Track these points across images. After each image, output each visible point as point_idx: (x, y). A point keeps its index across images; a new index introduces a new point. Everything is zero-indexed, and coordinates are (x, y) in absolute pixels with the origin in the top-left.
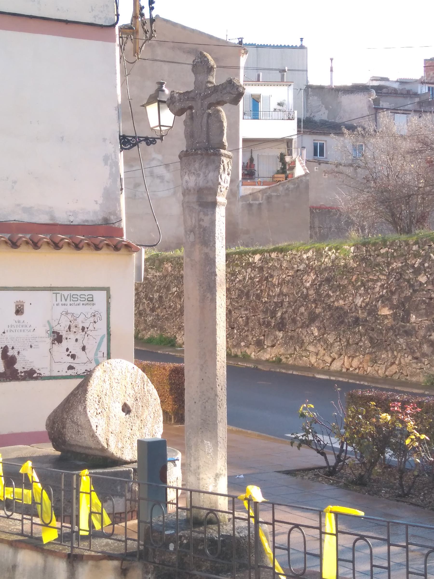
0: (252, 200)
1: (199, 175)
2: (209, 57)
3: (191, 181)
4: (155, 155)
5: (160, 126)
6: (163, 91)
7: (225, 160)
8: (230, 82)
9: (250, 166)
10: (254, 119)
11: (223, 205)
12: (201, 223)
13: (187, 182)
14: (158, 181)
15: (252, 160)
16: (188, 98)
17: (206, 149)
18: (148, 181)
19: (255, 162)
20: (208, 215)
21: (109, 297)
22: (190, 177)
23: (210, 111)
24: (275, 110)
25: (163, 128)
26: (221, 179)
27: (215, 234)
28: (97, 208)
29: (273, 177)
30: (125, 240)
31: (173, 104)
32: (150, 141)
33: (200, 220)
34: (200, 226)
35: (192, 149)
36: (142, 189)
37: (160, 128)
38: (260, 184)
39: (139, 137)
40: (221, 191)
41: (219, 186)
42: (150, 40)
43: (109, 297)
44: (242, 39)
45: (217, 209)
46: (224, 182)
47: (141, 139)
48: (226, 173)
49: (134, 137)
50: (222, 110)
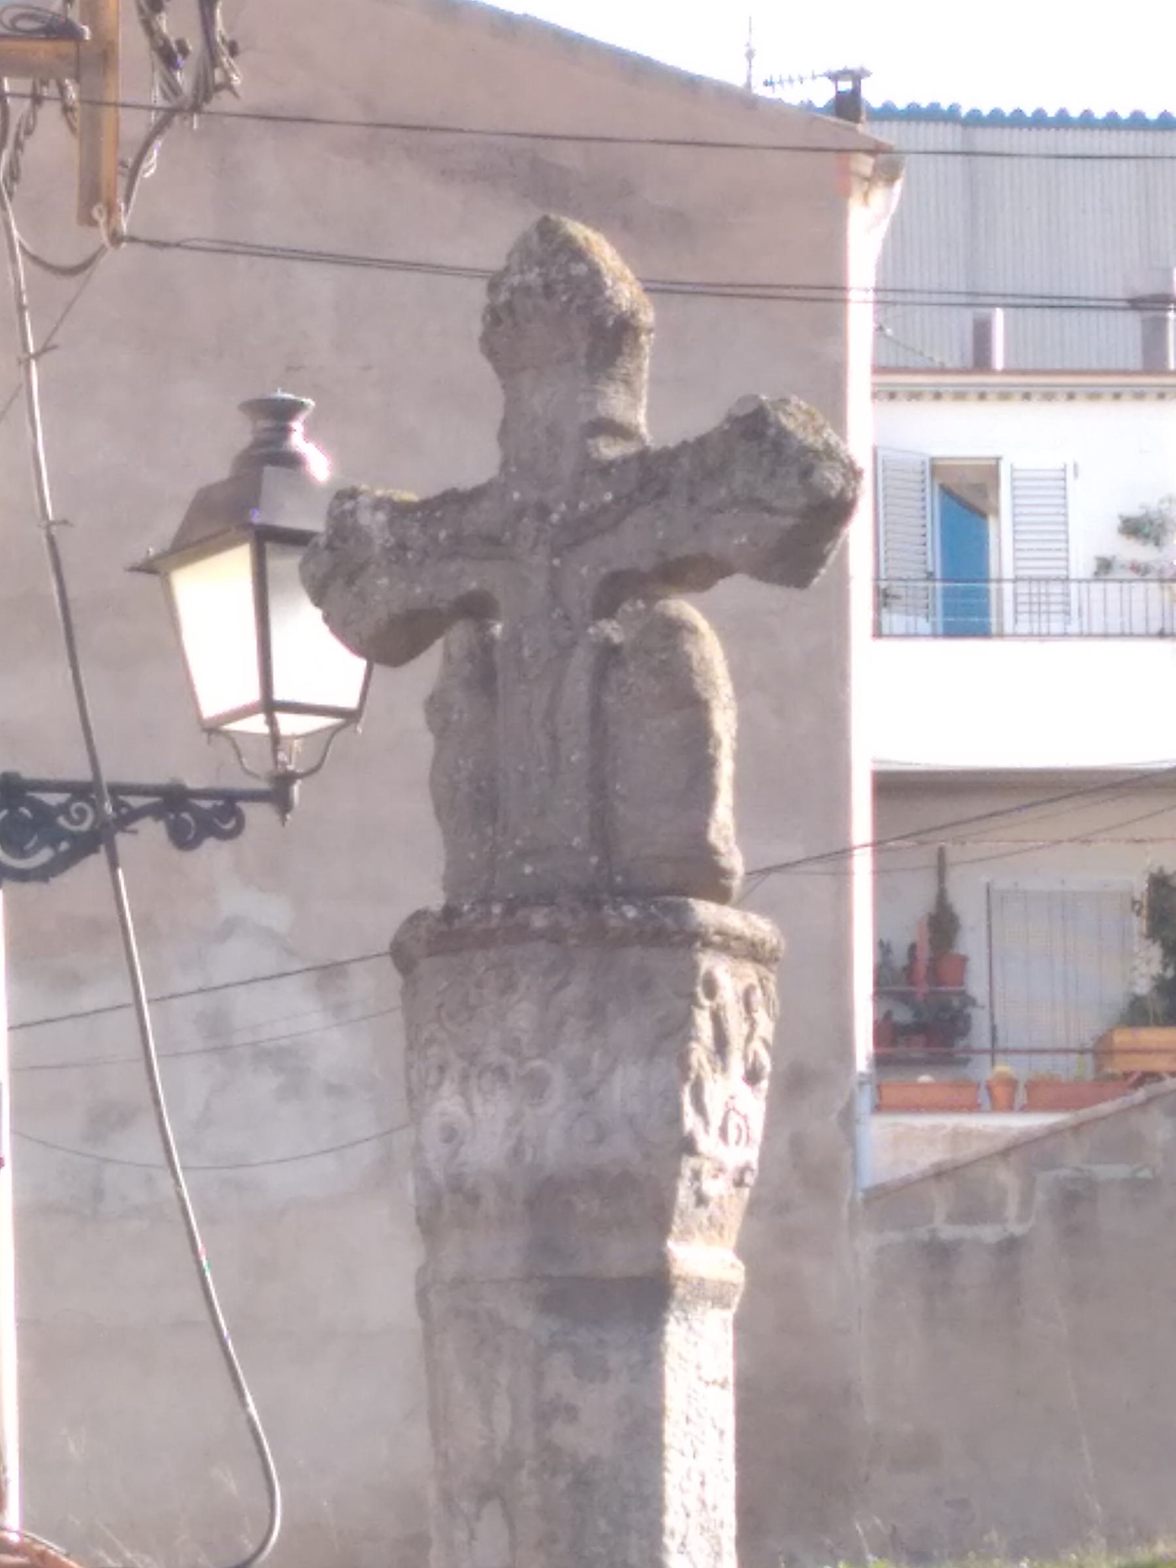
0: (952, 1219)
1: (537, 1086)
2: (606, 254)
3: (484, 1126)
4: (236, 900)
5: (269, 706)
6: (293, 461)
7: (729, 977)
8: (754, 428)
9: (935, 973)
10: (952, 632)
11: (720, 1301)
12: (564, 1434)
13: (450, 1135)
14: (266, 1083)
15: (943, 924)
16: (457, 539)
17: (592, 897)
18: (184, 1086)
19: (971, 943)
20: (605, 1373)
22: (477, 1100)
23: (613, 630)
24: (1105, 567)
25: (289, 724)
26: (700, 1108)
27: (660, 1510)
29: (1102, 1050)
30: (14, 1538)
31: (350, 580)
32: (196, 816)
33: (550, 1412)
34: (551, 1457)
35: (485, 900)
36: (138, 1144)
37: (272, 722)
38: (1004, 1097)
39: (117, 790)
40: (701, 1200)
41: (688, 1164)
42: (196, 108)
44: (857, 77)
45: (675, 1332)
46: (723, 1132)
47: (136, 802)
48: (737, 1066)
49: (81, 791)
50: (703, 625)
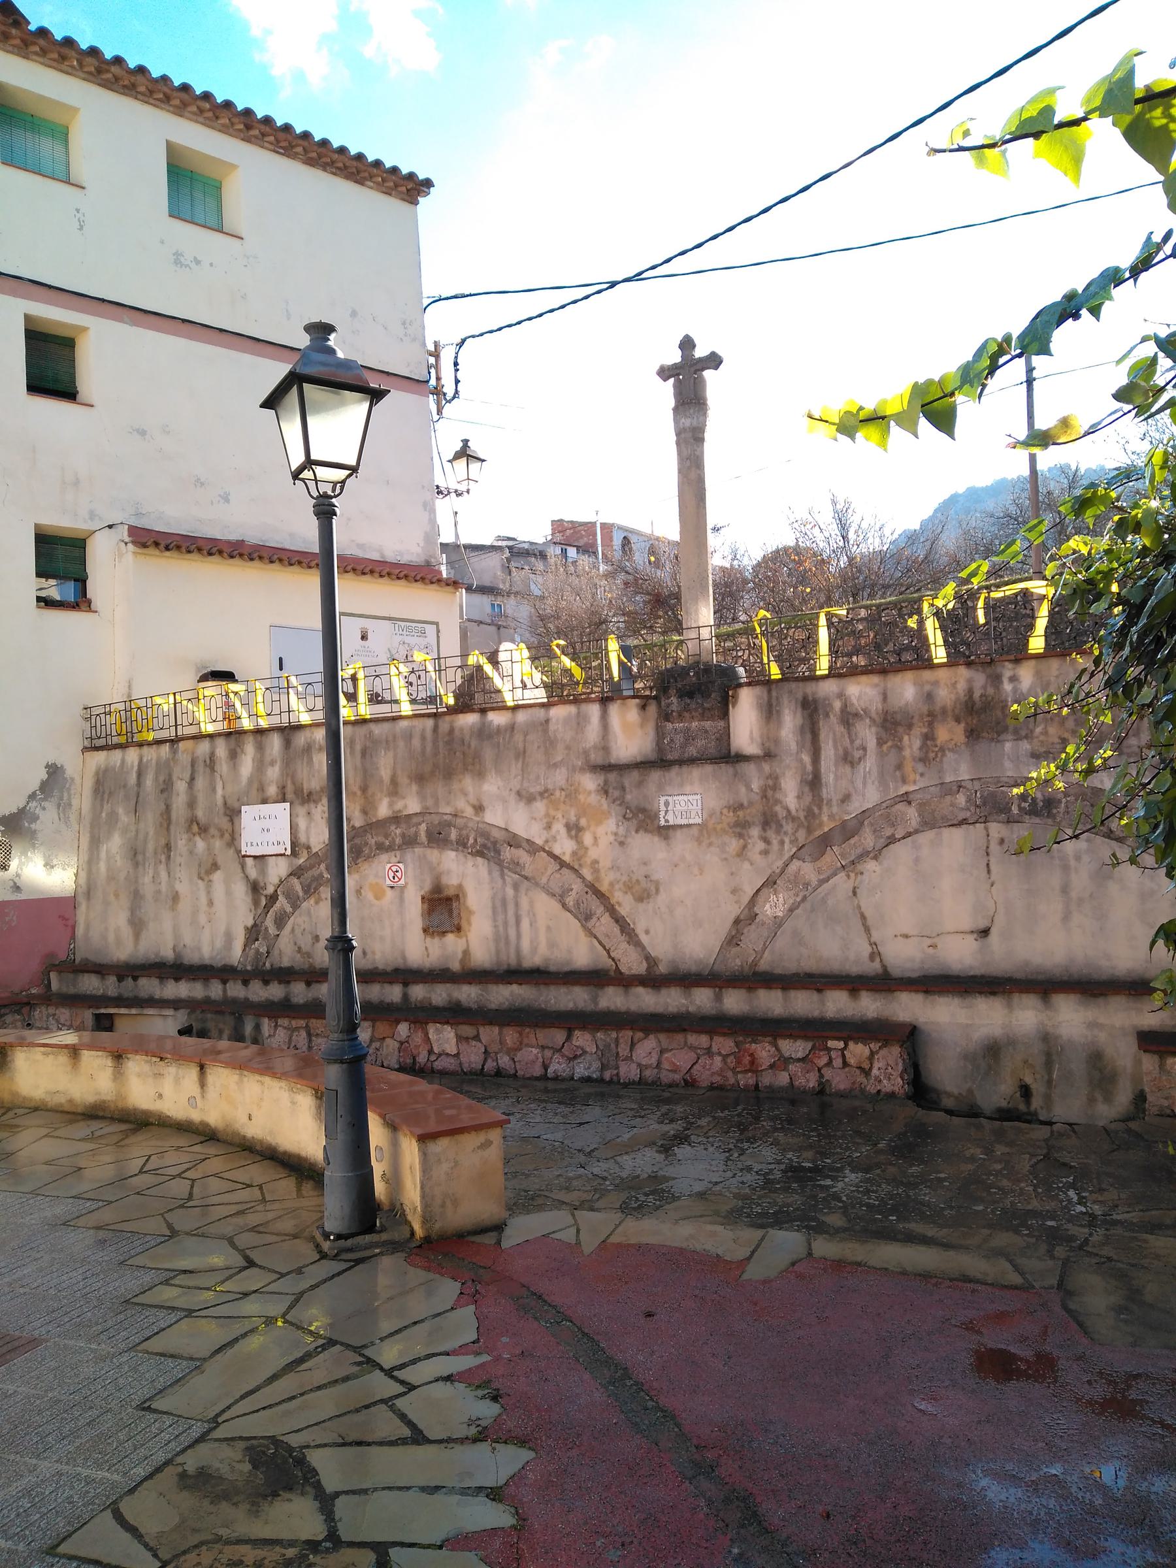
21: (438, 631)
25: (322, 473)
28: (419, 550)
43: (438, 631)
